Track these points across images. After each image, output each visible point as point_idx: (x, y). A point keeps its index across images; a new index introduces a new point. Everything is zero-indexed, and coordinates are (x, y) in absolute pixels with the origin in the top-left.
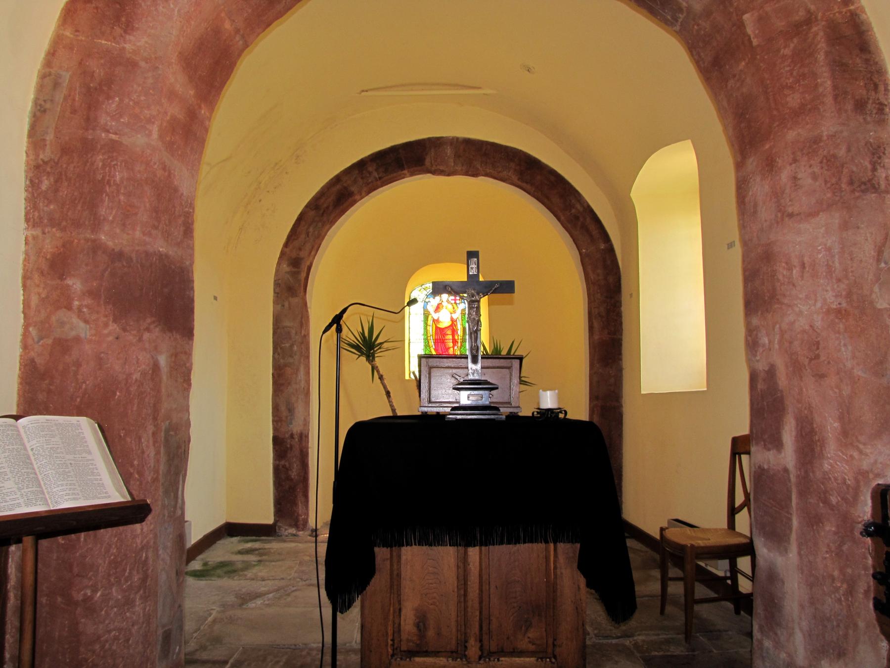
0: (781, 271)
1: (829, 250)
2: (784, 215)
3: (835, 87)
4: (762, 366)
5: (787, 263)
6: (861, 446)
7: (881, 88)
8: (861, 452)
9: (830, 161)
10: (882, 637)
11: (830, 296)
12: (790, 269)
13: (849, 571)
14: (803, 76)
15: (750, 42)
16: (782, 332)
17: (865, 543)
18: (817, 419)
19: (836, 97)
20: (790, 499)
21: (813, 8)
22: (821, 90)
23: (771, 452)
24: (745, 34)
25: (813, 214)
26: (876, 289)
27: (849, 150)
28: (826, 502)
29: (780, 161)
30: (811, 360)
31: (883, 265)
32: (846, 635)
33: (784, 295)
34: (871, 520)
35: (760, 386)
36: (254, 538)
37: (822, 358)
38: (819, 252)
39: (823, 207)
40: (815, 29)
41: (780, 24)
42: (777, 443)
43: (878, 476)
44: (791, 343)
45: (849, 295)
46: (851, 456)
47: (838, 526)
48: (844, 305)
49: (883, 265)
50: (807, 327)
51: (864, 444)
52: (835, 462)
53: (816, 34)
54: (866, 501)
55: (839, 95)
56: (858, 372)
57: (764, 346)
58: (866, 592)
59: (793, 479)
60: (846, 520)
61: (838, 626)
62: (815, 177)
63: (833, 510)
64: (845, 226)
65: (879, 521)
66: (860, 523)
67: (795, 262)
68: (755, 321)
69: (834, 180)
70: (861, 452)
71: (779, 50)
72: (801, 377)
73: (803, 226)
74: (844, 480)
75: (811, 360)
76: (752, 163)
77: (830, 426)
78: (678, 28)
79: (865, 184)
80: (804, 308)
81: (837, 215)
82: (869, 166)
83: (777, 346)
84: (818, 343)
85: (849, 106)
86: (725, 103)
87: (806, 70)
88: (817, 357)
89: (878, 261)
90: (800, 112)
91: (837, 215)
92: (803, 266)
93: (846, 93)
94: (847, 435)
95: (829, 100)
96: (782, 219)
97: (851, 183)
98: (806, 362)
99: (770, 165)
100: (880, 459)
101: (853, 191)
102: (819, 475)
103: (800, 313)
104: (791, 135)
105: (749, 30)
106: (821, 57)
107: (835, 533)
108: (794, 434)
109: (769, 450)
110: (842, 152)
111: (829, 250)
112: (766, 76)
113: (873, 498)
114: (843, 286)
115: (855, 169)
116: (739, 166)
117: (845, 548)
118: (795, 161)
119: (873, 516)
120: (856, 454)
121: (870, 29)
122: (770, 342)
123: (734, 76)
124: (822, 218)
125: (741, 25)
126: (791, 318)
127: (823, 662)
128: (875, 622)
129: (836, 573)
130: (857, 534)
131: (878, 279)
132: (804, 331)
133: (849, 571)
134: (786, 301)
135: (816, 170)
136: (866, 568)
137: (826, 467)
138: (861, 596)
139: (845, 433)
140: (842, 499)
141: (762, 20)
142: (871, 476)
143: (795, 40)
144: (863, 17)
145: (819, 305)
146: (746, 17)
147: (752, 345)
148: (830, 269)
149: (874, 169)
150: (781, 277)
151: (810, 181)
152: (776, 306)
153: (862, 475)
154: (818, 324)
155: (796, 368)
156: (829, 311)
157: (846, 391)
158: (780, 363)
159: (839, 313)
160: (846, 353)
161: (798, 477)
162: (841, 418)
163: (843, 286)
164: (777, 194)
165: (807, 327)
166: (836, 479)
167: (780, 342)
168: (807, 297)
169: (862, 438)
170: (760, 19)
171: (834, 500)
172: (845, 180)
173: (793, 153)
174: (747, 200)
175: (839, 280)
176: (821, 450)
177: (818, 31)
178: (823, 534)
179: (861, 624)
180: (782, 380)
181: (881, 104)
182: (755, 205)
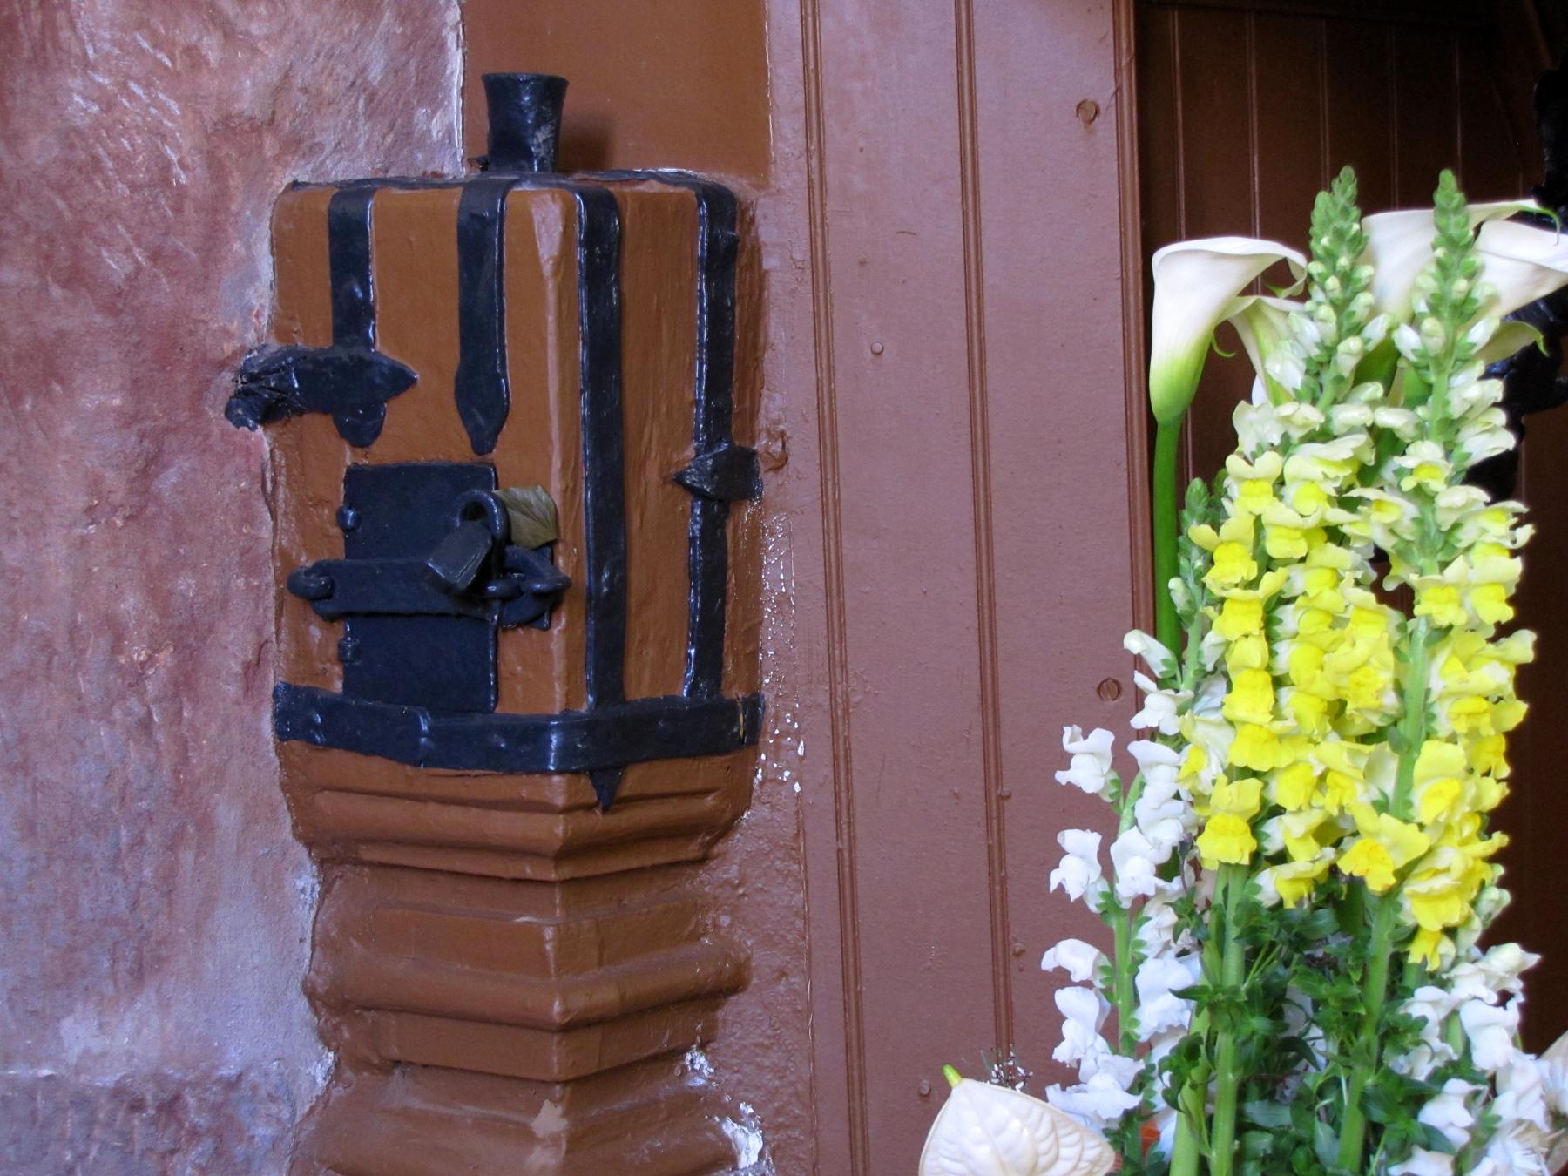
8: (229, 34)
10: (300, 851)
13: (186, 584)
17: (248, 452)
28: (77, 277)
32: (168, 881)
34: (274, 346)
36: (453, 772)
43: (294, 145)
46: (191, 51)
47: (136, 387)
54: (251, 259)
58: (252, 669)
60: (162, 353)
61: (139, 842)
63: (113, 312)
65: (316, 336)
66: (221, 365)
70: (229, 34)
107: (128, 420)
113: (279, 247)
117: (168, 481)
119: (279, 328)
127: (67, 1024)
128: (278, 796)
129: (131, 604)
130: (214, 413)
133: (186, 584)
136: (250, 567)
137: (80, 106)
138: (233, 690)
140: (156, 256)
142: (270, 146)
166: (124, 162)
171: (116, 265)
176: (49, 26)
178: (68, 429)
179: (228, 816)
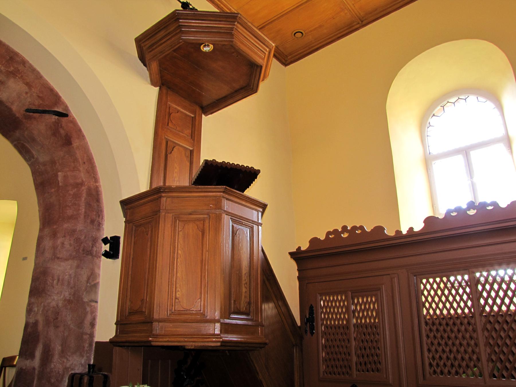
0: (49, 280)
1: (70, 275)
2: (55, 258)
3: (85, 212)
4: (32, 321)
5: (52, 277)
6: (68, 357)
7: (101, 217)
8: (67, 360)
9: (78, 240)
11: (67, 294)
12: (53, 280)
14: (75, 204)
15: (59, 184)
16: (44, 306)
18: (53, 345)
19: (85, 216)
20: (33, 382)
21: (84, 180)
22: (80, 212)
23: (28, 361)
24: (57, 179)
25: (67, 260)
26: (85, 293)
27: (85, 237)
28: (49, 382)
29: (59, 235)
30: (54, 320)
31: (89, 284)
33: (49, 291)
35: (29, 330)
37: (59, 319)
38: (66, 275)
39: (73, 258)
40: (83, 188)
41: (71, 181)
42: (32, 356)
43: (72, 369)
44: (47, 312)
45: (74, 294)
46: (64, 361)
48: (72, 298)
49: (89, 284)
50: (55, 306)
51: (69, 356)
52: (56, 364)
53: (83, 190)
55: (86, 216)
56: (72, 326)
57: (35, 311)
59: (36, 372)
62: (70, 245)
64: (78, 267)
67: (56, 278)
68: (33, 300)
69: (77, 248)
71: (69, 191)
72: (49, 327)
73: (62, 264)
74: (59, 372)
75: (54, 320)
76: (47, 231)
77: (57, 348)
78: (30, 163)
79: (88, 252)
80: (56, 298)
81: (76, 262)
82: (91, 246)
83: (41, 312)
84: (59, 313)
85: (89, 221)
86: (41, 201)
87: (77, 202)
88: (57, 318)
89: (87, 282)
90: (71, 217)
91: (76, 262)
92: (59, 280)
93: (88, 215)
94: (63, 353)
95: (82, 217)
96: (54, 259)
97: (83, 250)
98: (52, 320)
99: (54, 235)
100: (74, 363)
101: (84, 254)
102: (48, 370)
103: (54, 299)
104: (66, 226)
105: (60, 179)
106: (83, 199)
108: (41, 352)
109: (27, 360)
110: (83, 238)
111: (70, 275)
112: (61, 199)
114: (72, 291)
115: (86, 245)
116: (41, 230)
118: (65, 236)
120: (65, 360)
121: (101, 194)
122: (38, 310)
123: (49, 193)
124: (70, 262)
125: (57, 176)
126: (50, 301)
131: (86, 289)
132: (54, 307)
134: (49, 293)
135: (72, 242)
137: (52, 366)
139: (63, 351)
141: (65, 177)
143: (76, 189)
144: (100, 189)
145: (62, 297)
146: (59, 173)
147: (29, 311)
148: (69, 283)
149: (92, 247)
150: (48, 283)
151: (68, 246)
152: (44, 295)
153: (66, 369)
154: (60, 305)
155: (47, 322)
156: (65, 300)
157: (66, 334)
158: (40, 319)
159: (69, 302)
160: (69, 318)
161: (39, 371)
162: (62, 345)
163: (72, 291)
164: (54, 248)
165: (55, 306)
167: (43, 311)
168: (58, 293)
169: (69, 354)
170: (65, 176)
171: (53, 381)
172: (81, 249)
173: (65, 233)
174: (41, 246)
175: (71, 288)
177: (84, 189)
180: (40, 327)
181: (100, 223)
182: (44, 249)
